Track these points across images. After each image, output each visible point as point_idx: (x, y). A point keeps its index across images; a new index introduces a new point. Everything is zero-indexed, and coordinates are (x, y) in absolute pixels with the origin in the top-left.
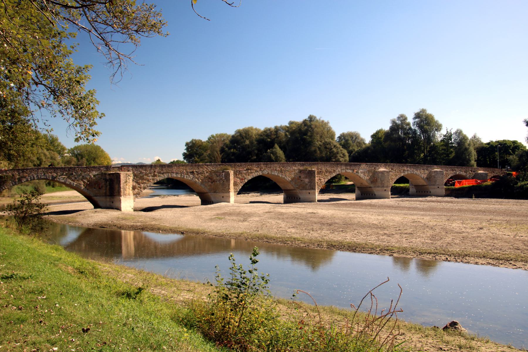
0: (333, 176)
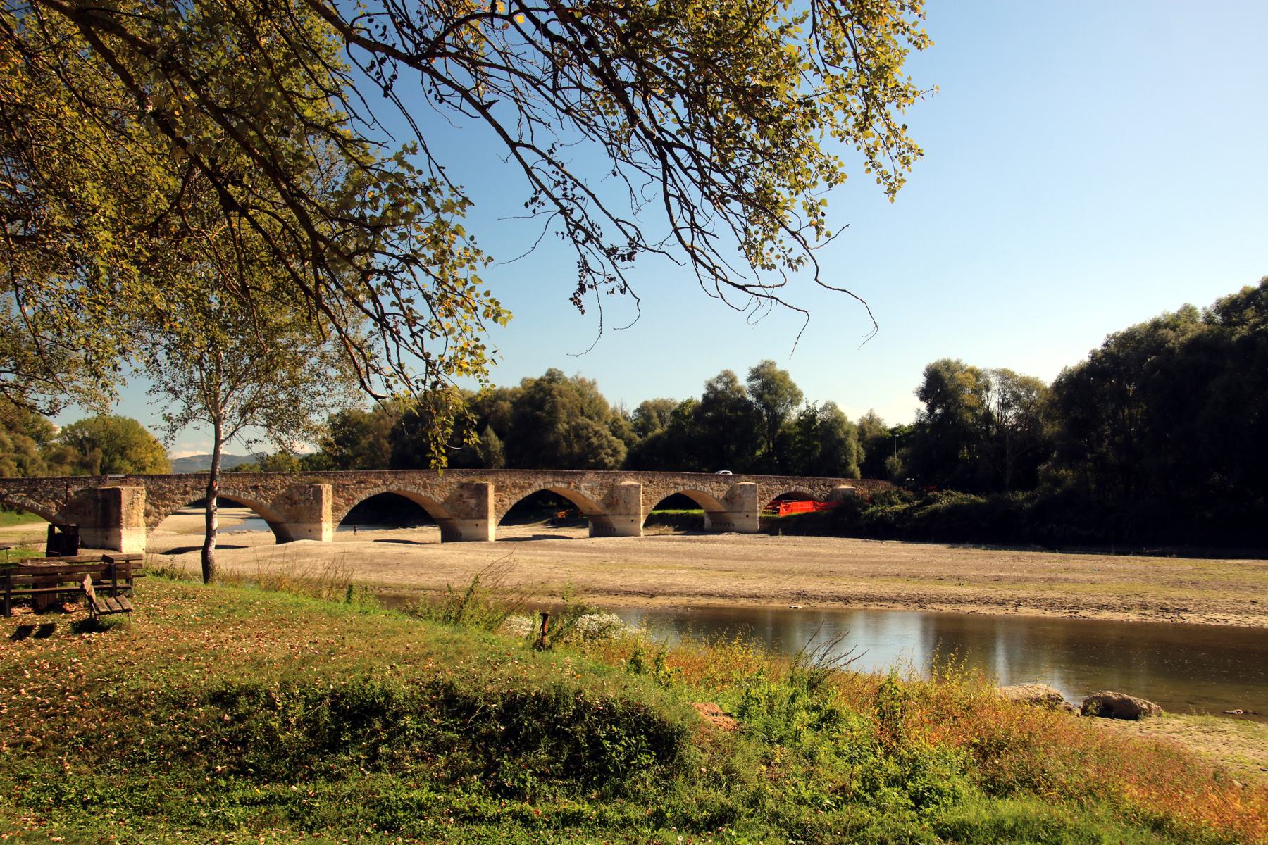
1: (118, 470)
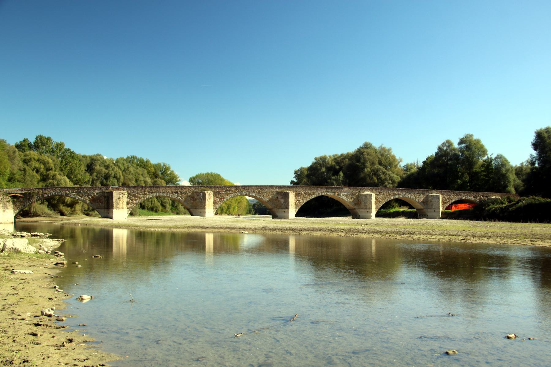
0: (312, 198)
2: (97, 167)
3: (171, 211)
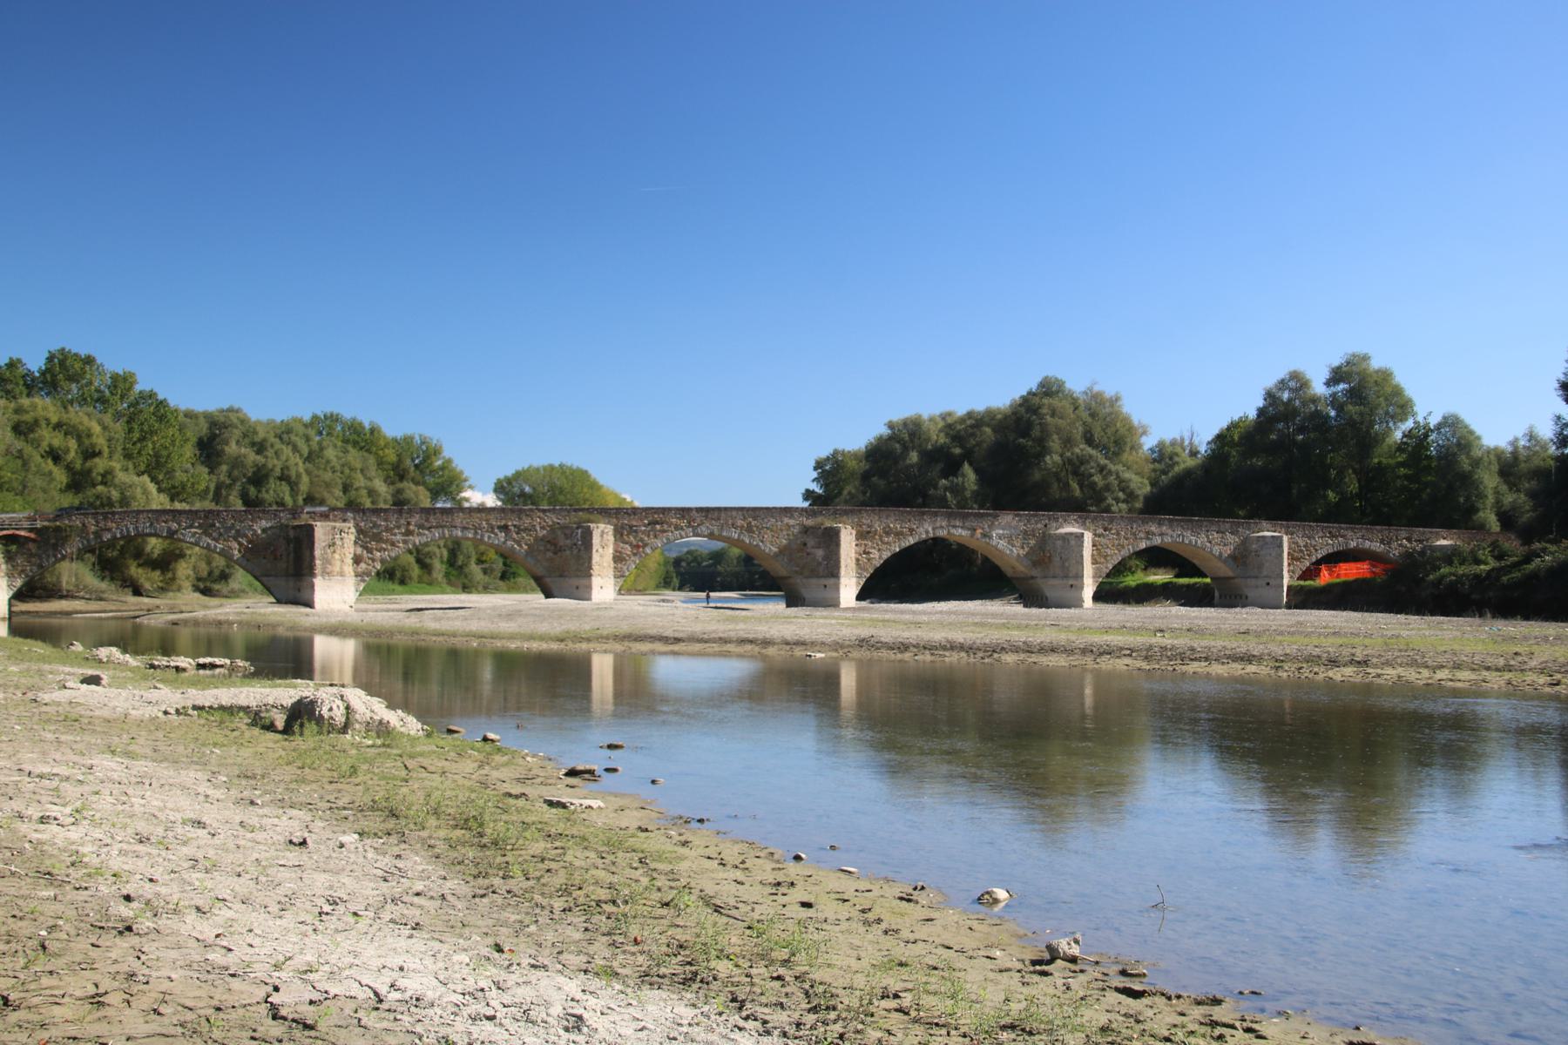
0: (908, 544)
1: (322, 503)
2: (232, 449)
3: (445, 581)
